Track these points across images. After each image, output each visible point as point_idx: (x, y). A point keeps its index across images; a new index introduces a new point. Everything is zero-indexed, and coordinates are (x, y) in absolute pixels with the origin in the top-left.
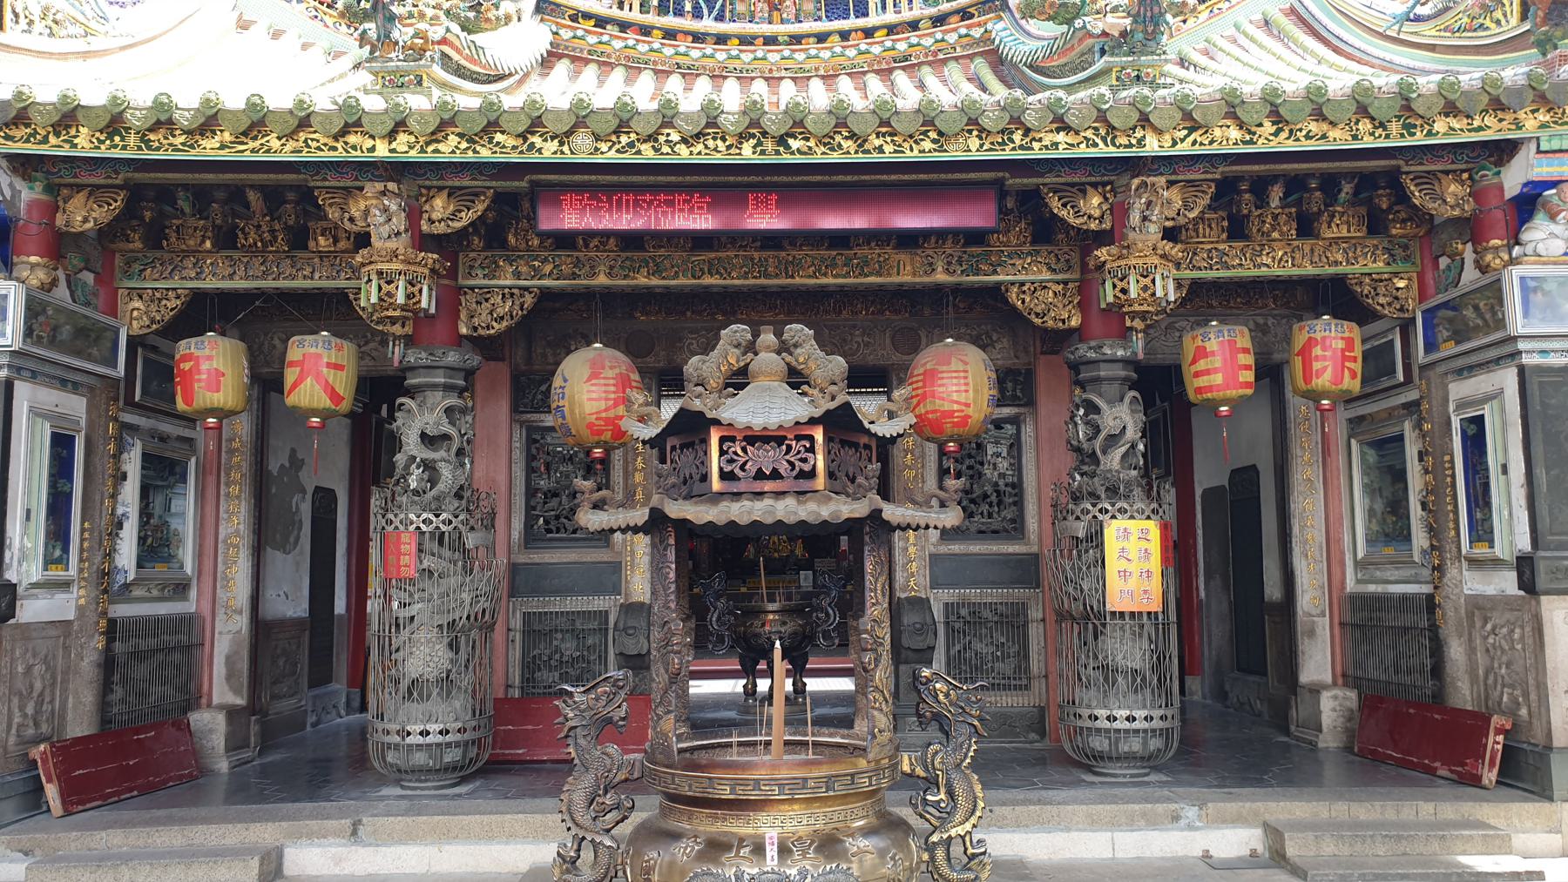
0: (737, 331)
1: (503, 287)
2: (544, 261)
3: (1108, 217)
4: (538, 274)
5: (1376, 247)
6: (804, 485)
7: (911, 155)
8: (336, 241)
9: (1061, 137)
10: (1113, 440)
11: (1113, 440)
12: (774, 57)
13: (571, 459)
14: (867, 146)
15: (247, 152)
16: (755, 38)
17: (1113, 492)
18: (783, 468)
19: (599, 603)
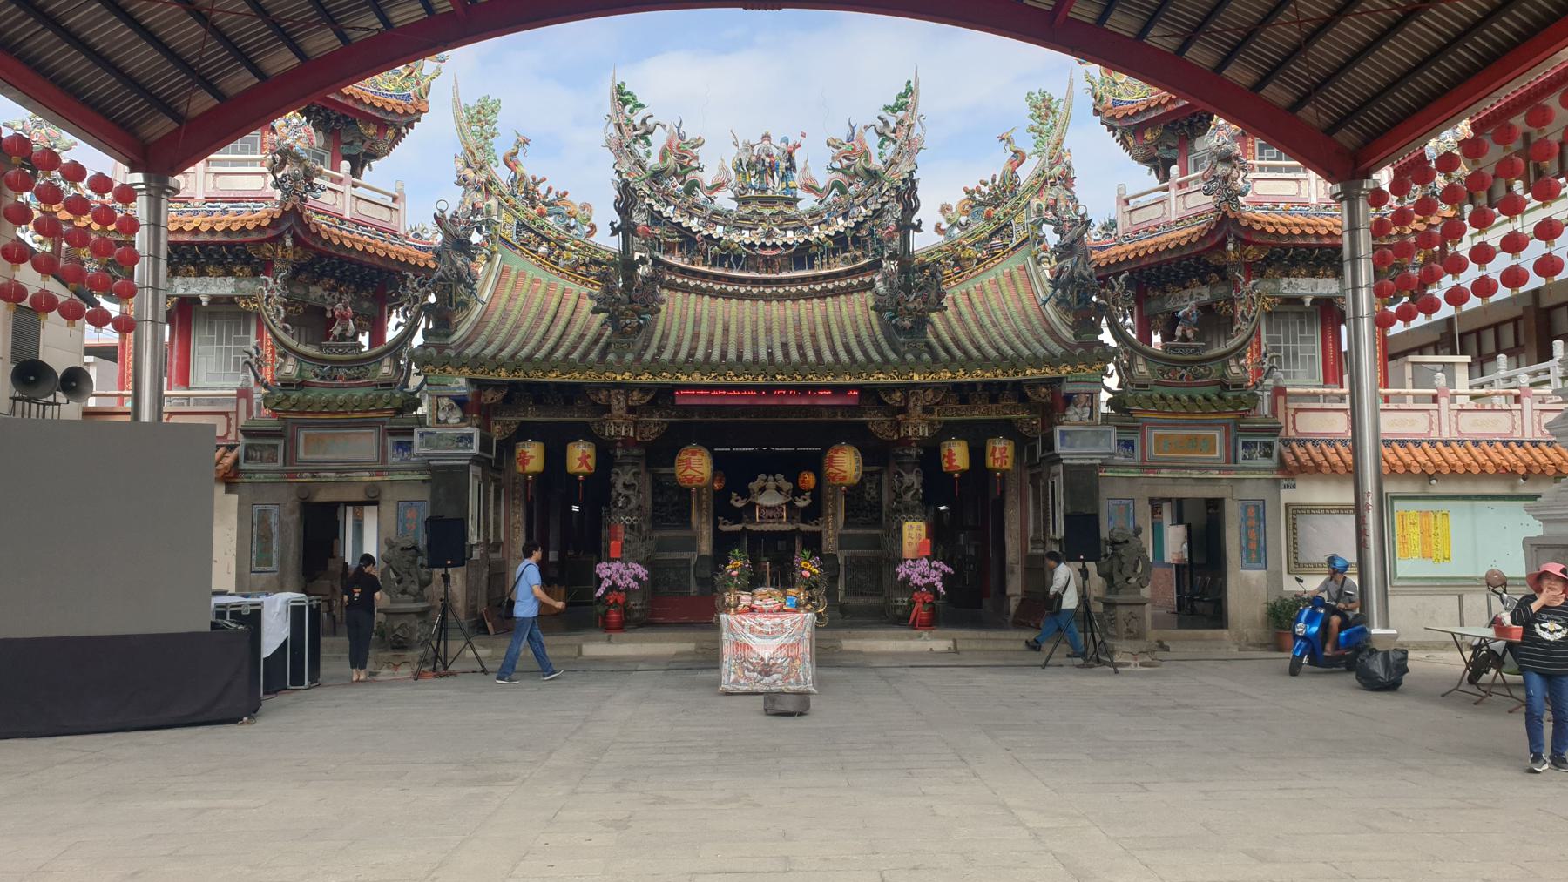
0: (763, 476)
10: (908, 488)
11: (908, 488)
15: (566, 379)
17: (907, 510)
19: (686, 555)
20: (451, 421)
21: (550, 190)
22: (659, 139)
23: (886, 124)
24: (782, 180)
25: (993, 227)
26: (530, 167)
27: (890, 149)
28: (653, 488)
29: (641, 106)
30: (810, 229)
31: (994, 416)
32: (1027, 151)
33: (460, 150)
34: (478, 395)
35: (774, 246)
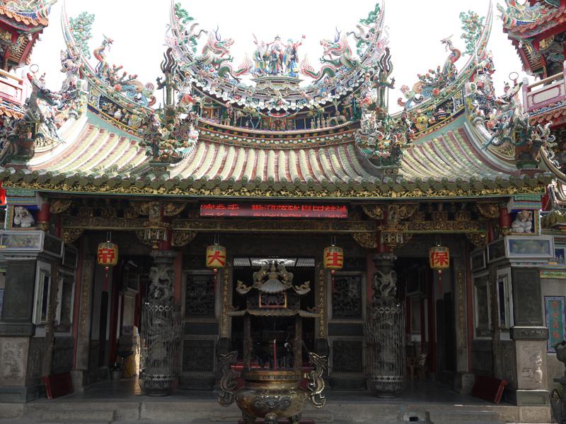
1: (185, 231)
2: (200, 222)
3: (382, 216)
4: (198, 227)
5: (474, 224)
6: (281, 306)
7: (319, 197)
8: (133, 215)
9: (366, 193)
10: (386, 286)
11: (386, 286)
12: (277, 143)
13: (202, 286)
14: (305, 194)
16: (270, 135)
17: (385, 304)
18: (276, 302)
20: (23, 225)
21: (125, 74)
22: (202, 42)
23: (362, 30)
24: (288, 66)
25: (438, 101)
26: (111, 59)
27: (364, 49)
28: (188, 285)
29: (191, 19)
30: (308, 100)
31: (452, 231)
32: (462, 52)
33: (65, 48)
34: (48, 207)
35: (282, 111)
